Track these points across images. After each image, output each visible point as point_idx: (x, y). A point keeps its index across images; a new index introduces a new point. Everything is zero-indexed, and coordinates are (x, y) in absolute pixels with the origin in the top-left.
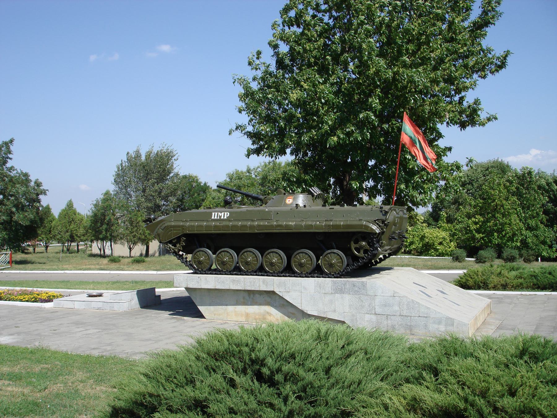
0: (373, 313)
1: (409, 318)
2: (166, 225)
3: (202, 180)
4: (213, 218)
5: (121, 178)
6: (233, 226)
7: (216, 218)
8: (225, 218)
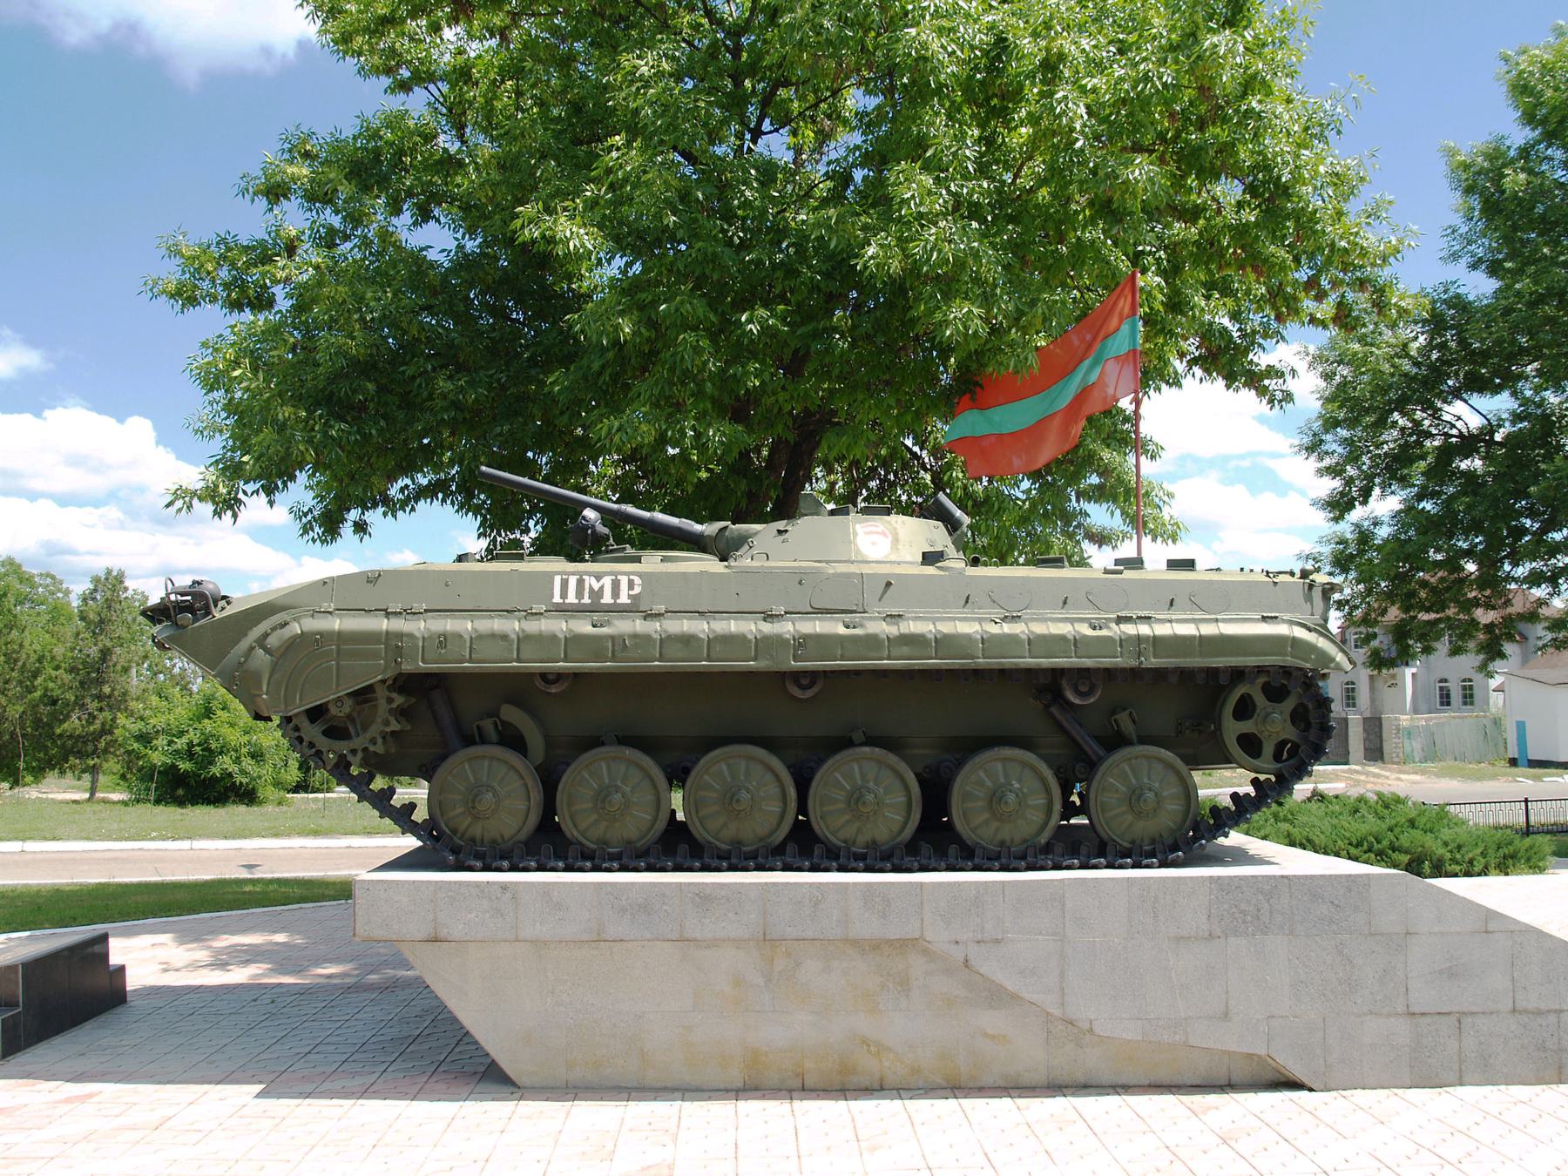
0: (1401, 1009)
1: (1552, 1018)
2: (296, 628)
3: (60, 410)
4: (557, 599)
5: (1237, 390)
6: (668, 640)
7: (572, 598)
8: (624, 599)
